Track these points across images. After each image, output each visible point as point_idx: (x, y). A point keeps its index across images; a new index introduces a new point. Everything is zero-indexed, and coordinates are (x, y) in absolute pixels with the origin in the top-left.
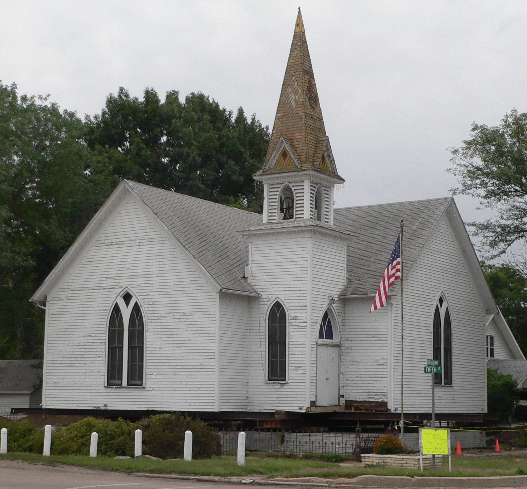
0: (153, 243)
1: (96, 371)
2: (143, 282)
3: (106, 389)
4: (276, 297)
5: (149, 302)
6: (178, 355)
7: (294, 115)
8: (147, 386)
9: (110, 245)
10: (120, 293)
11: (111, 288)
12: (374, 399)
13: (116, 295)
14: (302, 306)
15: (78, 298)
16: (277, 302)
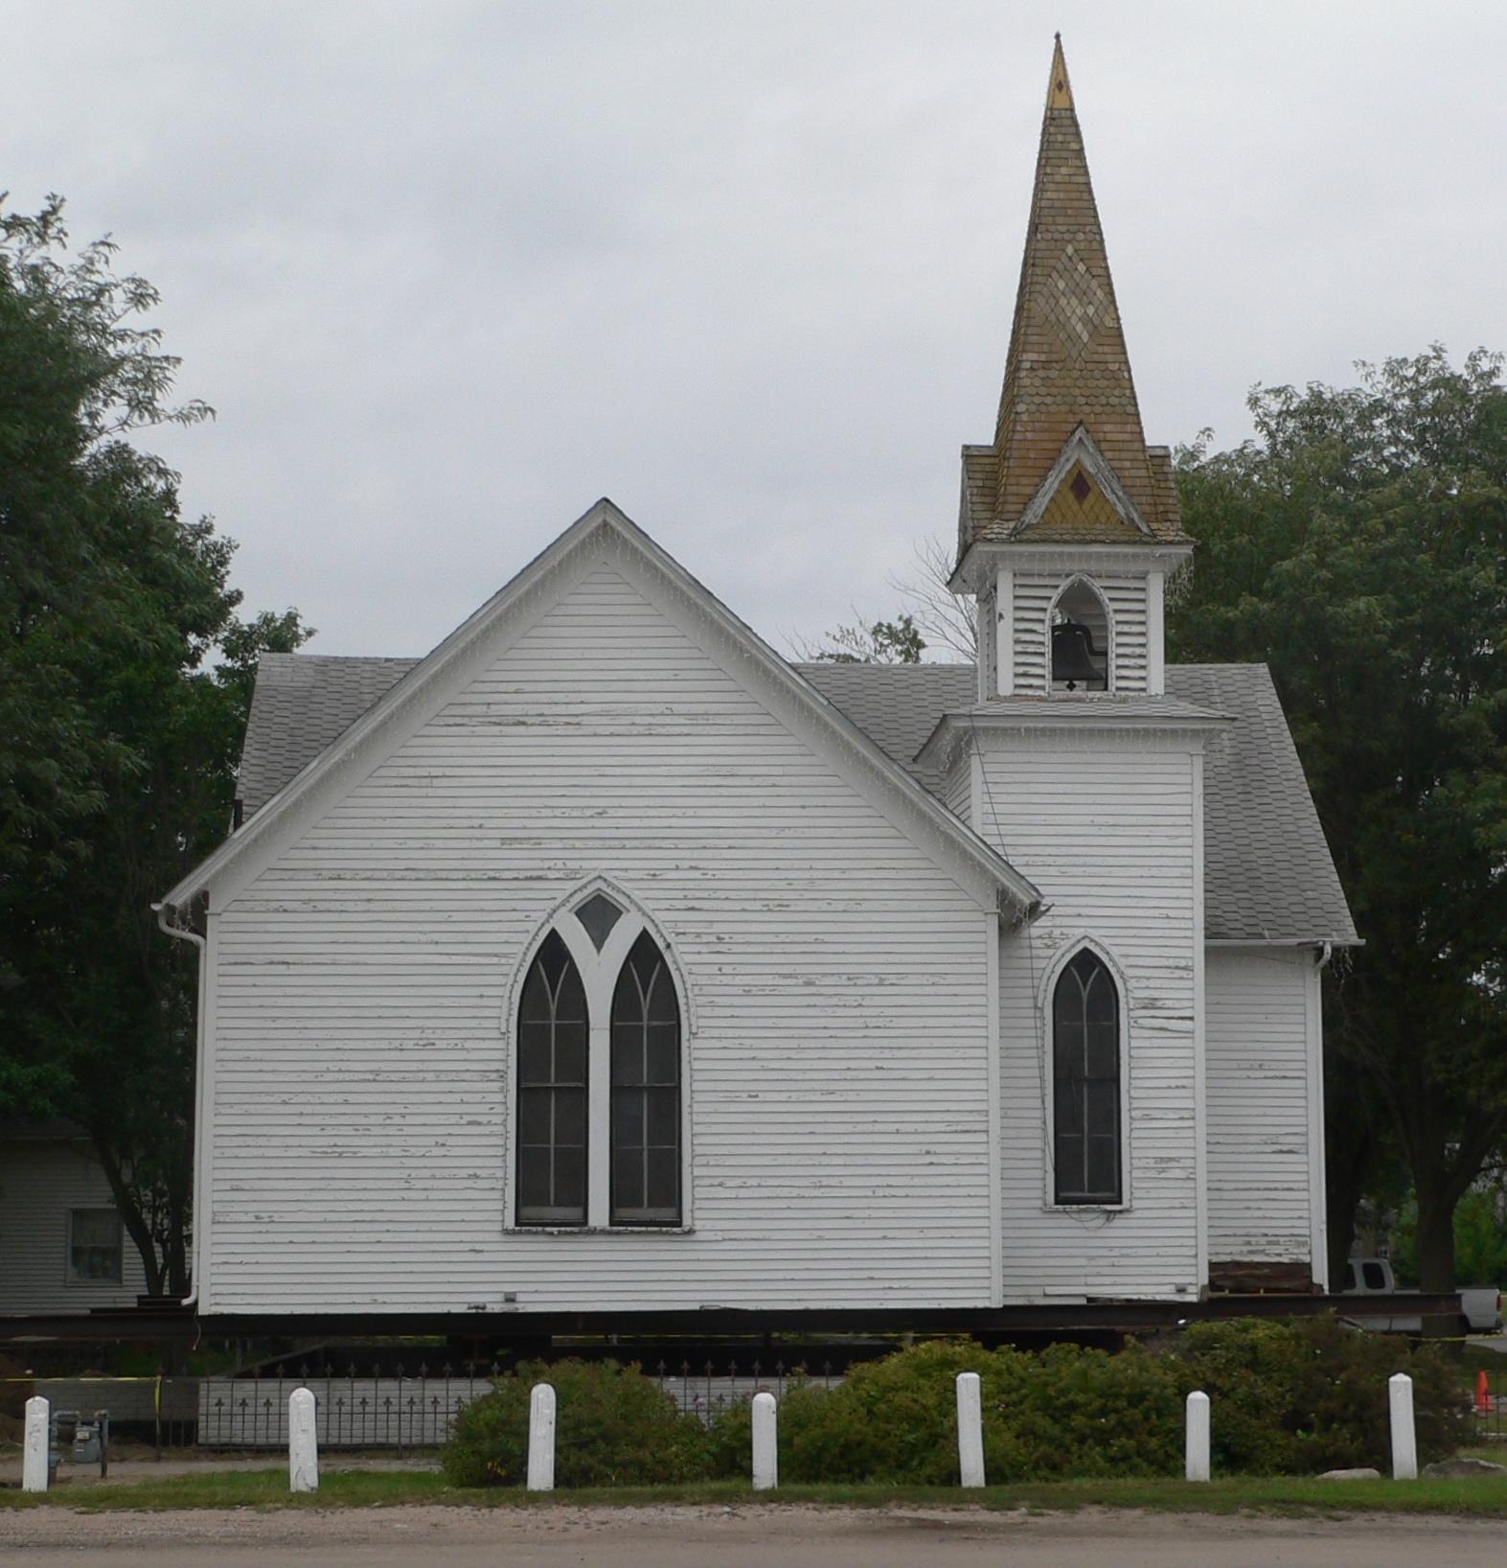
0: (712, 730)
1: (464, 1173)
2: (672, 864)
3: (1047, 1216)
4: (1079, 937)
5: (698, 935)
6: (829, 1118)
7: (1090, 366)
8: (698, 1225)
9: (515, 724)
10: (571, 895)
11: (527, 879)
12: (1268, 1255)
13: (552, 904)
14: (1177, 968)
15: (362, 906)
16: (1086, 950)
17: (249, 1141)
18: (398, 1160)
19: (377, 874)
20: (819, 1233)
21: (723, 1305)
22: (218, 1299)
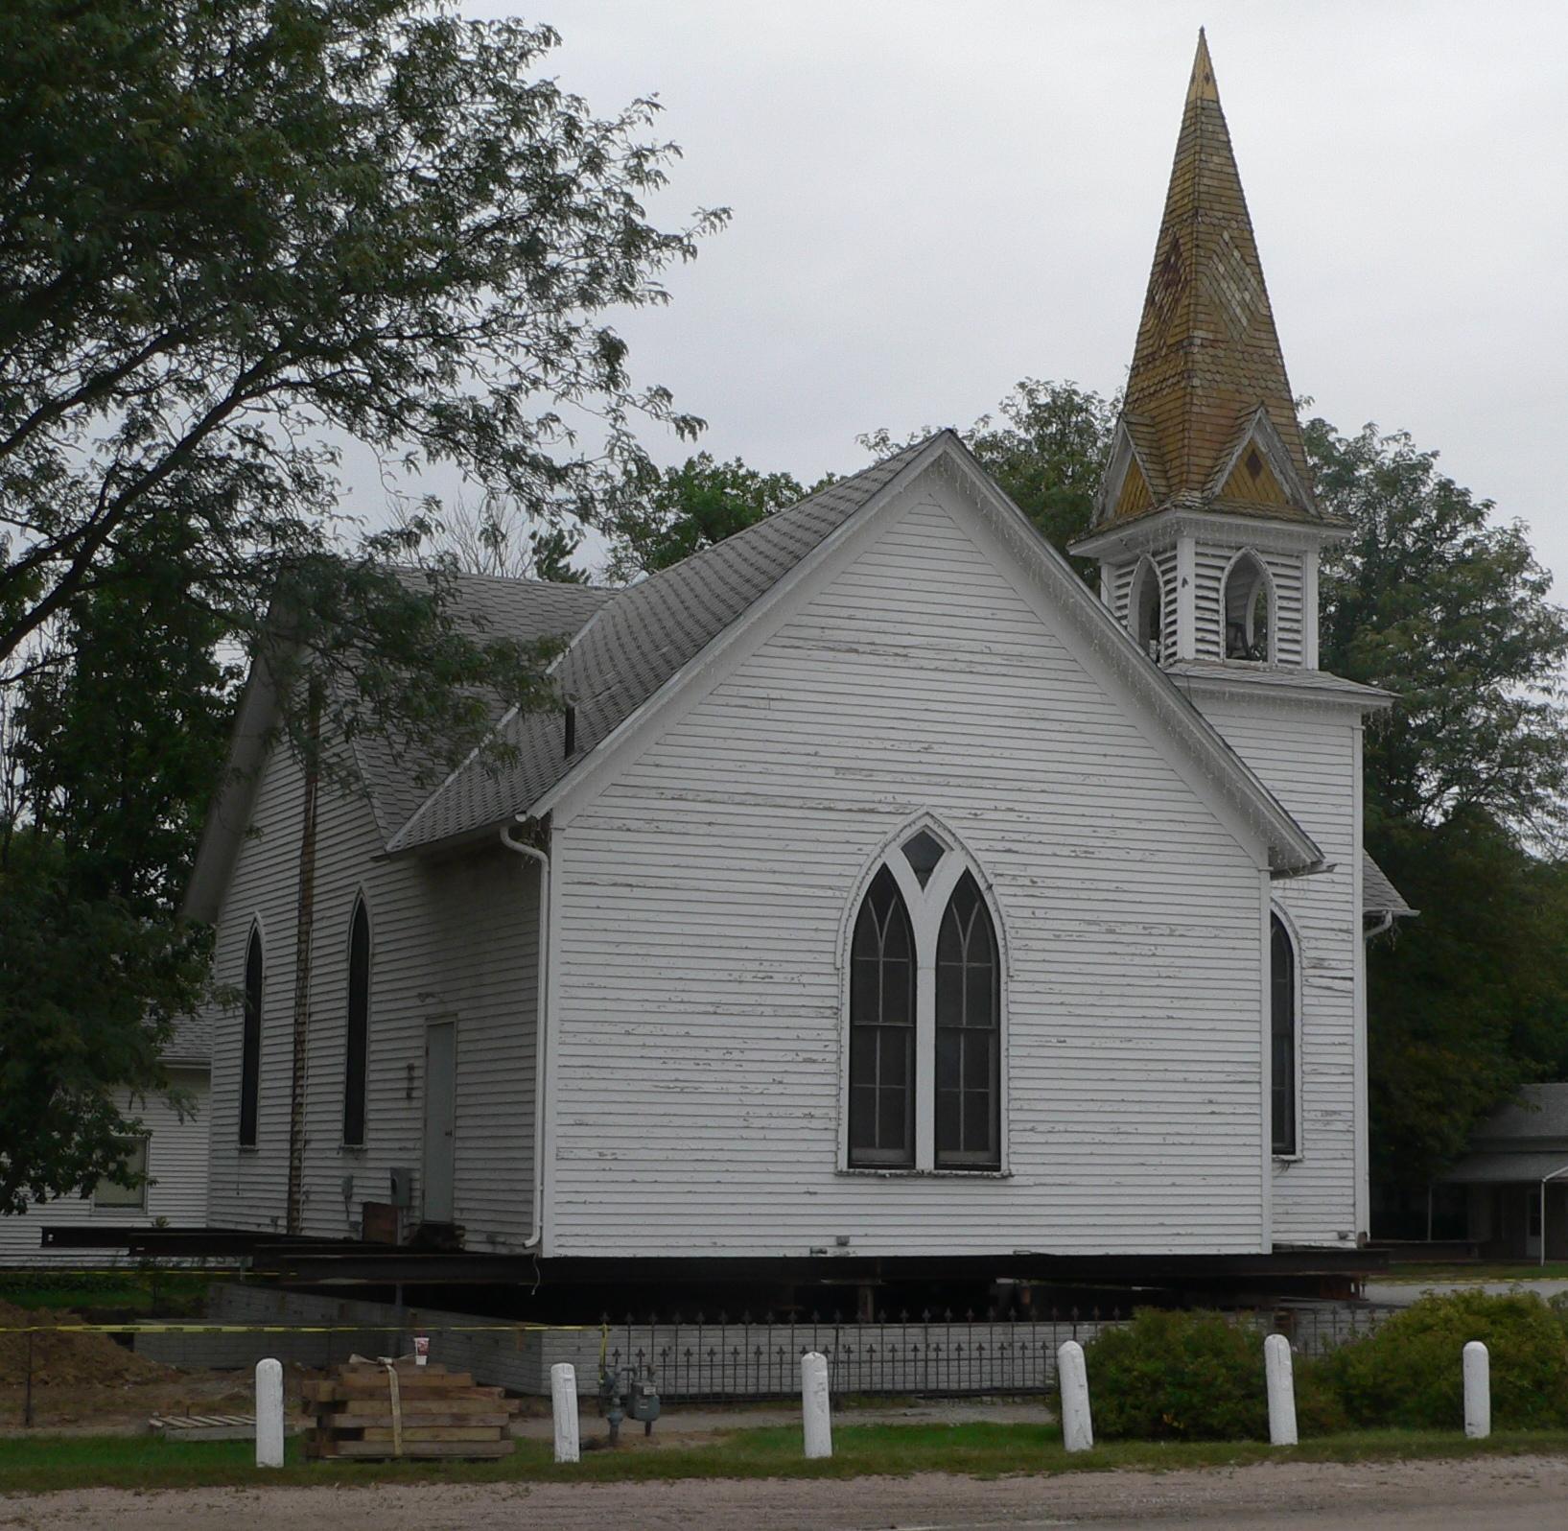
1: (799, 1112)
3: (842, 1180)
5: (1014, 877)
7: (1251, 350)
13: (884, 839)
14: (1341, 930)
15: (705, 829)
17: (593, 1073)
18: (737, 1097)
19: (718, 797)
20: (1117, 1179)
21: (1034, 1250)
22: (563, 1241)
